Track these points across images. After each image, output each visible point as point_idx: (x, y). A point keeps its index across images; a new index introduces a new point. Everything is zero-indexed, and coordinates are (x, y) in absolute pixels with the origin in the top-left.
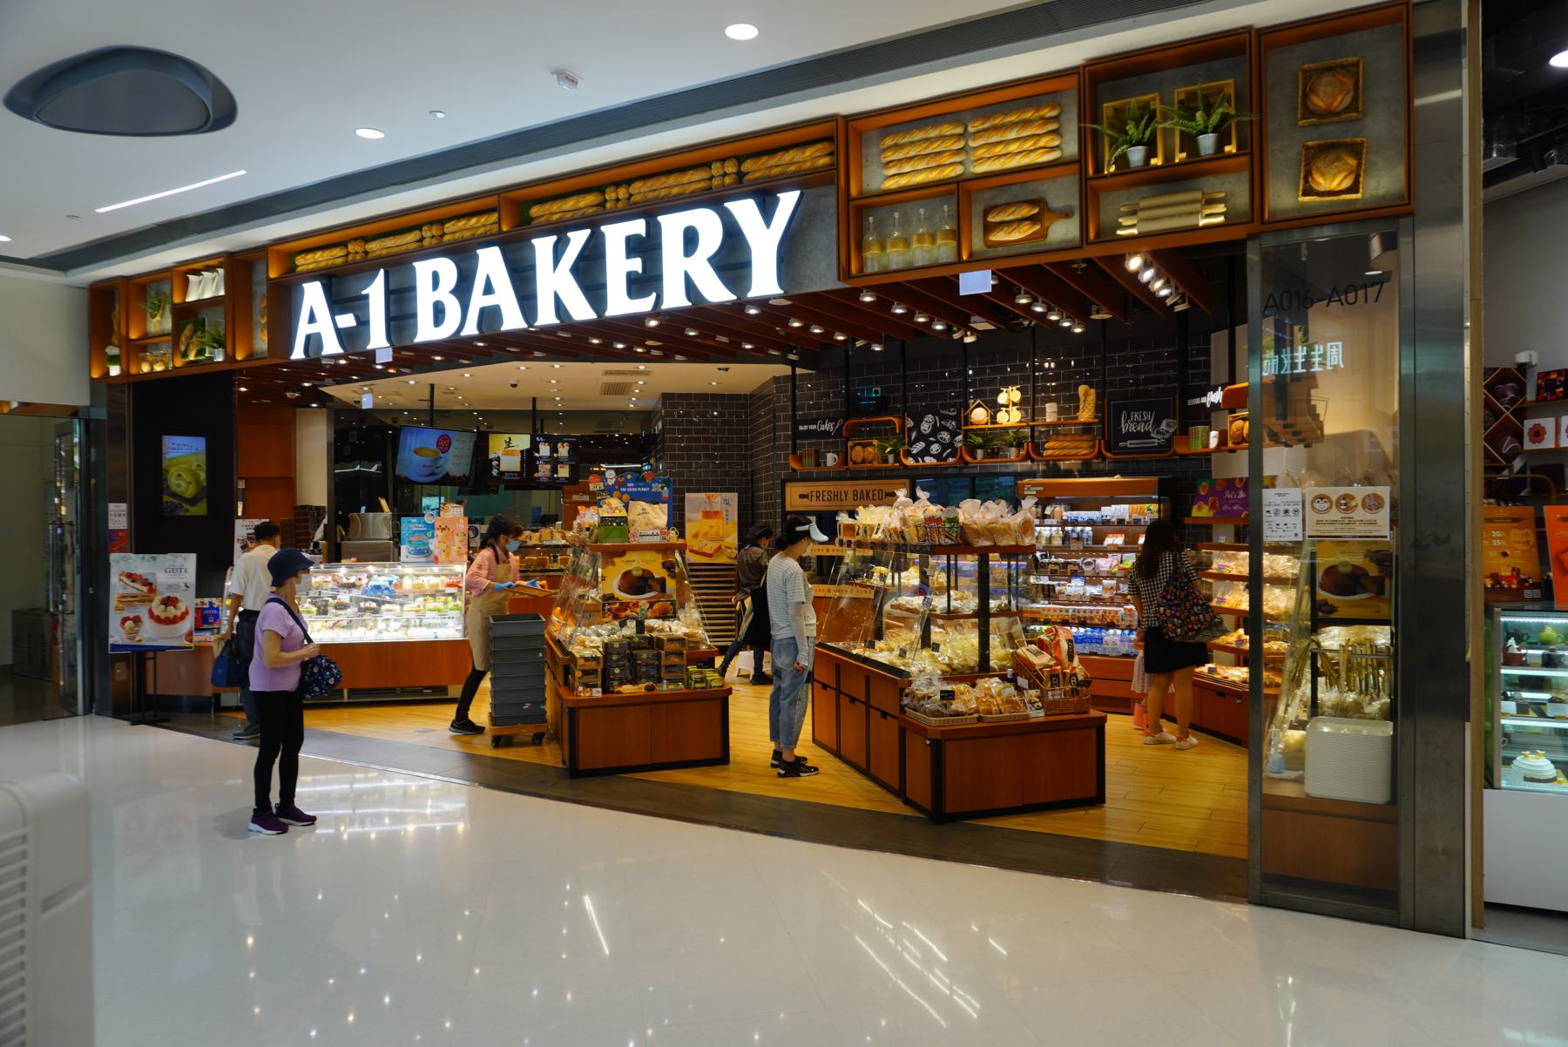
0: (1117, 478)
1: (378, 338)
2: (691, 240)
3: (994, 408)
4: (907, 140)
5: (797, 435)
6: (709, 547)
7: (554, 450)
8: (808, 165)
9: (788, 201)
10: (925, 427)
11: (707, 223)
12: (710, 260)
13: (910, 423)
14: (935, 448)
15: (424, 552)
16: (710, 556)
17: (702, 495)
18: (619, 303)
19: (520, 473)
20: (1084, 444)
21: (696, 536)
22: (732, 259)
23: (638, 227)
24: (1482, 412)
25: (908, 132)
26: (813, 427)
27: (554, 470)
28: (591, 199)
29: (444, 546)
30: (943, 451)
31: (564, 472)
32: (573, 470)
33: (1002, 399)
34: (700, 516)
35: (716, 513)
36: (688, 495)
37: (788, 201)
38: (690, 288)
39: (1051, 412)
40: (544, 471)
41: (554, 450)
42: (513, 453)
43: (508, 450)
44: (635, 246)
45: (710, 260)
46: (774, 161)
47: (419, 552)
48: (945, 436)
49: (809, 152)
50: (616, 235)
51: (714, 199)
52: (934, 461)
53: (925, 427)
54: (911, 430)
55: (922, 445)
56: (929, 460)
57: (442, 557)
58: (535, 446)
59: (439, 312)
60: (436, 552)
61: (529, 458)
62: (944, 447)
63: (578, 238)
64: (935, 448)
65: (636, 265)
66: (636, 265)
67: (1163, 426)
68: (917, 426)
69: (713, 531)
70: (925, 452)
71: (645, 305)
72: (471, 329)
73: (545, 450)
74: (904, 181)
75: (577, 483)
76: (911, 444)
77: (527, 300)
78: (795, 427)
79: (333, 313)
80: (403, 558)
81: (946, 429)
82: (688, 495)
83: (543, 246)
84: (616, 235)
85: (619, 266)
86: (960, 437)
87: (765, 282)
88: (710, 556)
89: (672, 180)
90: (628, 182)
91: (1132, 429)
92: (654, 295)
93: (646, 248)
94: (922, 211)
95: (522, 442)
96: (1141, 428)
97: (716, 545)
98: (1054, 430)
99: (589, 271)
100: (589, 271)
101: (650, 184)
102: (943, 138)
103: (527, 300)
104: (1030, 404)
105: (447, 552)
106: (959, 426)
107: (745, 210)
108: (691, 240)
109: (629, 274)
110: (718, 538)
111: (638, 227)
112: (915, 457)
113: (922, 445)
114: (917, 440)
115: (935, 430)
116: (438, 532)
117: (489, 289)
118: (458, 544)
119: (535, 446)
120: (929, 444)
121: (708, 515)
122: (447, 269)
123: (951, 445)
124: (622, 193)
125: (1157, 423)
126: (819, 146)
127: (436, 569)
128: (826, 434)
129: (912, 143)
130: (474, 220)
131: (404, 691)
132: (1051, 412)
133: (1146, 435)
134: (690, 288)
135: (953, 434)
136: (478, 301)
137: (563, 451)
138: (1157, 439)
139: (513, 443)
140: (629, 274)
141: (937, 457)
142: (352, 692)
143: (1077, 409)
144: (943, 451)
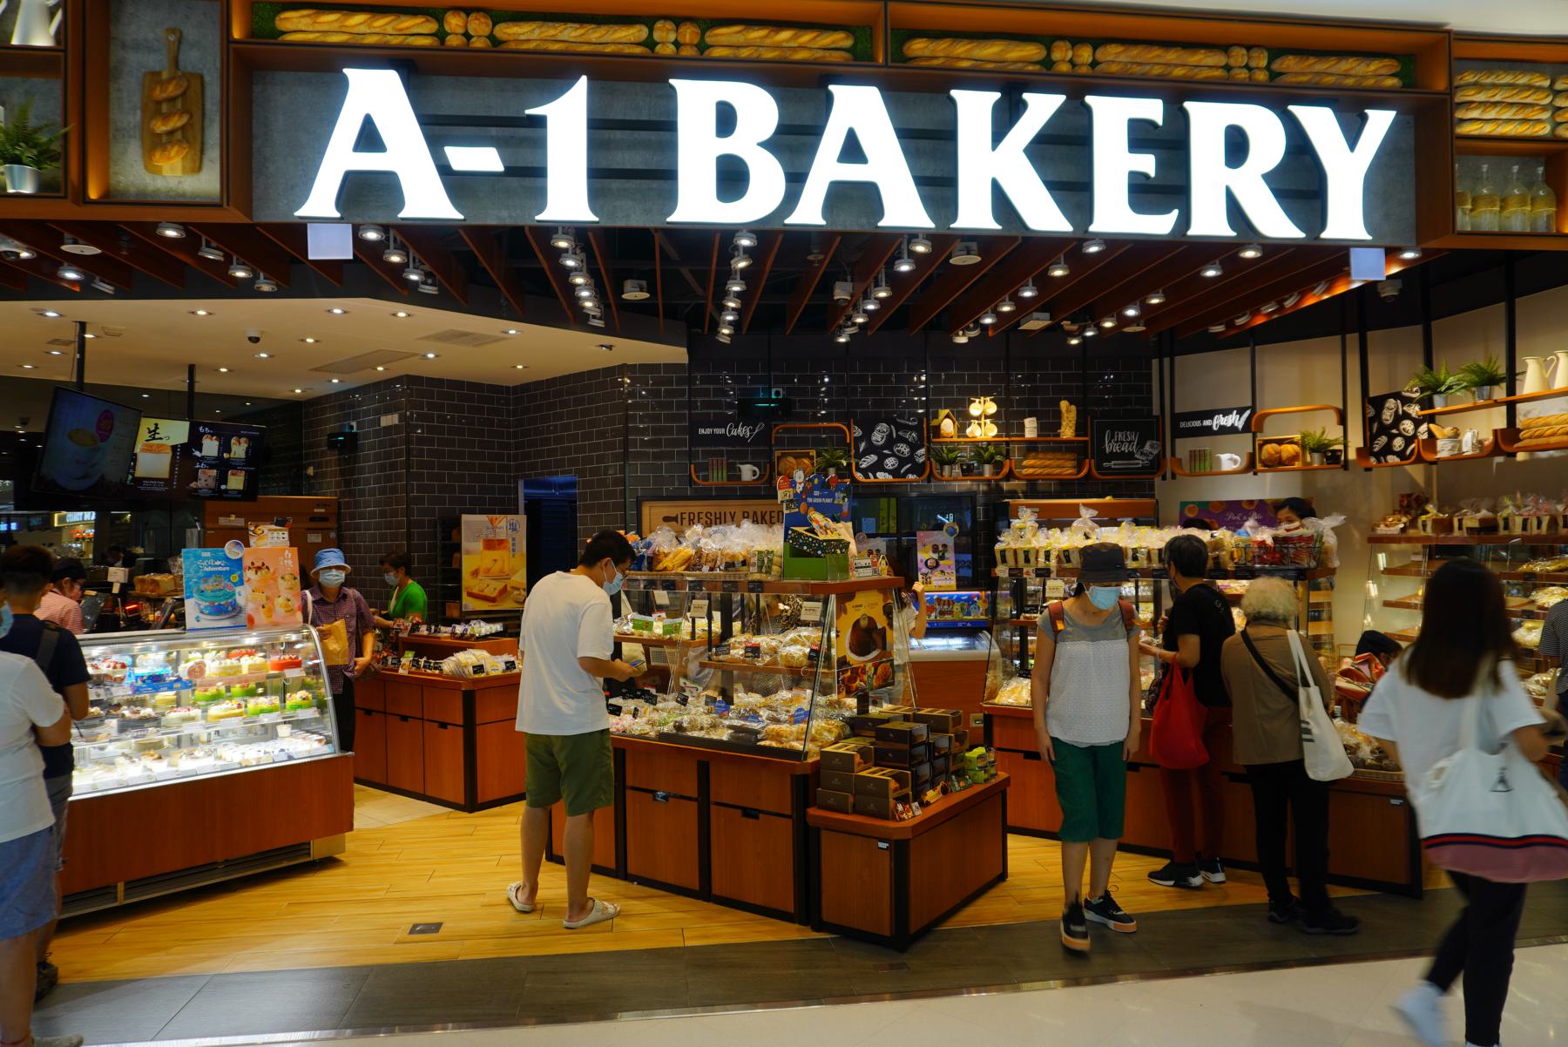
0: (1108, 499)
1: (567, 197)
2: (1237, 146)
3: (963, 419)
4: (1489, 81)
5: (697, 440)
6: (492, 588)
7: (225, 447)
8: (1370, 82)
9: (1380, 122)
10: (878, 437)
11: (1265, 130)
12: (1269, 178)
13: (858, 432)
14: (890, 462)
15: (227, 609)
16: (493, 600)
17: (484, 518)
18: (1114, 214)
19: (167, 482)
20: (1069, 464)
21: (475, 573)
22: (1301, 181)
23: (1152, 109)
24: (1059, 455)
25: (1490, 71)
26: (722, 431)
27: (222, 479)
28: (1031, 51)
29: (261, 598)
30: (901, 466)
31: (236, 482)
32: (250, 481)
33: (975, 409)
34: (480, 545)
35: (501, 542)
36: (465, 517)
37: (1380, 122)
38: (1235, 211)
39: (1030, 428)
40: (206, 478)
41: (225, 447)
42: (159, 450)
43: (157, 446)
44: (1140, 136)
45: (1269, 178)
46: (1321, 66)
47: (218, 610)
48: (904, 449)
49: (1375, 66)
50: (1112, 116)
51: (1278, 97)
52: (889, 478)
53: (878, 437)
54: (858, 440)
55: (873, 458)
56: (882, 476)
57: (260, 618)
58: (195, 440)
59: (732, 177)
60: (250, 608)
61: (184, 455)
62: (902, 461)
63: (1041, 107)
64: (890, 462)
65: (1147, 163)
66: (1147, 163)
67: (1147, 448)
68: (867, 435)
69: (497, 566)
70: (878, 466)
71: (1160, 224)
72: (809, 212)
73: (210, 447)
74: (1488, 129)
75: (254, 499)
76: (859, 456)
77: (938, 185)
78: (692, 430)
79: (436, 144)
80: (190, 622)
81: (905, 441)
82: (465, 517)
83: (974, 108)
84: (1112, 116)
85: (1115, 163)
86: (922, 451)
87: (1346, 218)
88: (493, 600)
89: (1172, 56)
90: (1098, 42)
91: (1116, 449)
92: (1176, 212)
93: (1168, 143)
94: (1515, 168)
95: (176, 432)
96: (1125, 448)
97: (500, 585)
98: (1031, 447)
99: (1065, 156)
100: (1065, 156)
101: (1135, 53)
102: (1528, 87)
103: (938, 185)
104: (1007, 419)
105: (268, 607)
106: (920, 436)
107: (1320, 123)
108: (1237, 146)
109: (1133, 175)
110: (504, 576)
111: (1152, 109)
112: (865, 472)
113: (873, 458)
114: (866, 452)
115: (891, 442)
116: (250, 574)
117: (852, 150)
118: (285, 594)
119: (195, 440)
120: (882, 458)
121: (491, 544)
122: (759, 110)
123: (911, 459)
124: (1085, 54)
125: (1141, 445)
126: (1386, 62)
127: (251, 640)
128: (739, 440)
129: (1494, 86)
130: (785, 35)
131: (230, 864)
132: (1030, 428)
133: (1130, 456)
134: (1235, 211)
135: (914, 447)
136: (826, 168)
137: (239, 449)
138: (1141, 461)
139: (162, 432)
140: (1133, 175)
141: (893, 472)
142: (131, 886)
143: (1059, 426)
144: (901, 466)
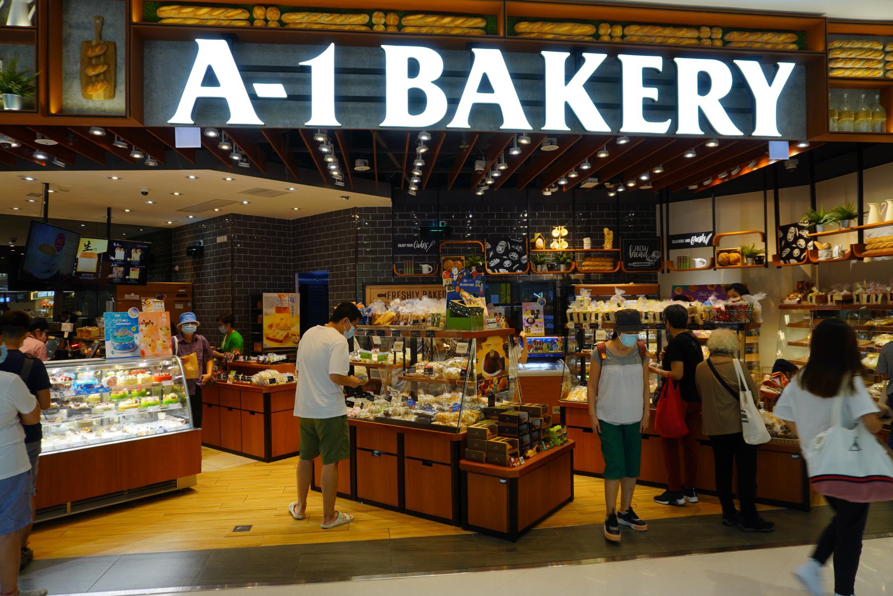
0: (631, 284)
1: (323, 112)
2: (704, 83)
3: (549, 239)
4: (848, 46)
5: (397, 251)
6: (280, 335)
7: (128, 254)
8: (780, 47)
9: (786, 69)
10: (500, 249)
11: (720, 74)
12: (723, 101)
13: (489, 246)
14: (507, 263)
15: (129, 347)
16: (281, 342)
17: (276, 295)
18: (634, 122)
19: (95, 274)
20: (609, 264)
21: (271, 326)
22: (741, 103)
23: (656, 62)
24: (603, 259)
25: (849, 41)
26: (411, 245)
27: (127, 273)
28: (587, 29)
29: (149, 340)
30: (513, 265)
31: (134, 274)
32: (143, 274)
33: (555, 233)
34: (273, 311)
35: (285, 308)
36: (265, 295)
37: (786, 69)
38: (703, 120)
39: (587, 243)
40: (117, 272)
41: (128, 254)
42: (90, 256)
43: (89, 254)
44: (649, 77)
45: (723, 101)
46: (753, 38)
47: (124, 347)
48: (515, 255)
49: (783, 37)
50: (633, 66)
51: (728, 55)
52: (507, 272)
53: (500, 249)
54: (488, 251)
55: (497, 261)
56: (502, 271)
57: (148, 352)
58: (111, 250)
59: (417, 101)
60: (142, 346)
61: (105, 259)
62: (514, 262)
63: (593, 61)
64: (507, 263)
65: (653, 93)
66: (653, 93)
67: (653, 255)
68: (494, 248)
69: (283, 322)
70: (500, 266)
71: (661, 128)
72: (461, 121)
73: (120, 254)
74: (847, 74)
75: (145, 284)
76: (489, 260)
77: (534, 105)
78: (394, 245)
79: (248, 82)
80: (108, 354)
81: (515, 251)
82: (265, 295)
83: (555, 62)
84: (633, 66)
85: (635, 93)
86: (525, 257)
87: (766, 124)
88: (281, 342)
89: (667, 32)
90: (625, 24)
91: (636, 256)
92: (670, 121)
93: (665, 81)
94: (863, 96)
95: (100, 246)
96: (641, 255)
97: (284, 333)
98: (587, 255)
99: (606, 89)
100: (606, 89)
101: (646, 30)
102: (870, 50)
103: (534, 105)
104: (574, 239)
105: (153, 345)
106: (524, 248)
107: (752, 70)
108: (704, 83)
109: (645, 100)
110: (287, 328)
111: (656, 62)
112: (492, 269)
113: (497, 261)
114: (493, 258)
115: (507, 252)
116: (142, 327)
117: (485, 86)
118: (162, 338)
119: (111, 250)
120: (503, 260)
121: (279, 310)
122: (432, 62)
123: (519, 261)
124: (618, 31)
125: (650, 253)
126: (790, 35)
127: (143, 364)
128: (421, 250)
129: (851, 49)
130: (447, 20)
131: (131, 492)
132: (587, 243)
133: (644, 259)
134: (703, 120)
135: (521, 255)
136: (471, 96)
137: (136, 256)
138: (650, 262)
139: (92, 246)
140: (645, 100)
141: (509, 269)
142: (75, 504)
143: (603, 242)
144: (513, 265)
